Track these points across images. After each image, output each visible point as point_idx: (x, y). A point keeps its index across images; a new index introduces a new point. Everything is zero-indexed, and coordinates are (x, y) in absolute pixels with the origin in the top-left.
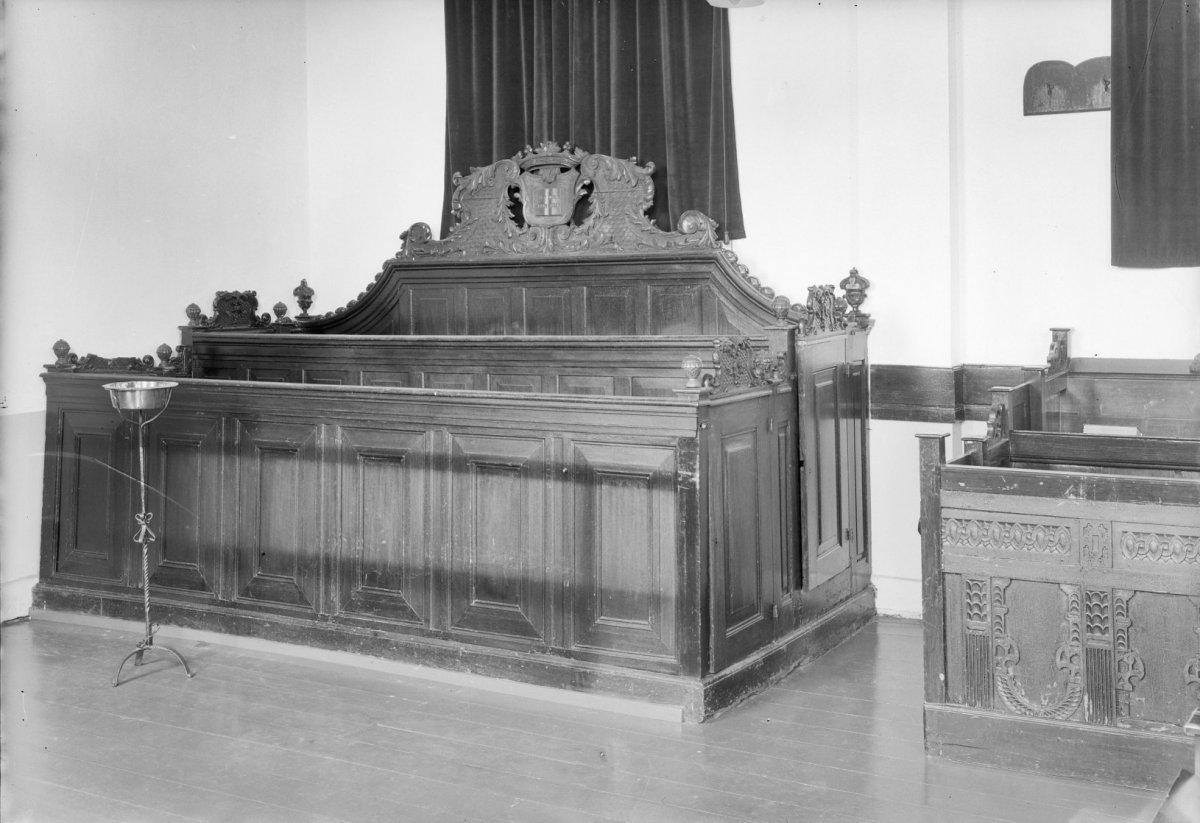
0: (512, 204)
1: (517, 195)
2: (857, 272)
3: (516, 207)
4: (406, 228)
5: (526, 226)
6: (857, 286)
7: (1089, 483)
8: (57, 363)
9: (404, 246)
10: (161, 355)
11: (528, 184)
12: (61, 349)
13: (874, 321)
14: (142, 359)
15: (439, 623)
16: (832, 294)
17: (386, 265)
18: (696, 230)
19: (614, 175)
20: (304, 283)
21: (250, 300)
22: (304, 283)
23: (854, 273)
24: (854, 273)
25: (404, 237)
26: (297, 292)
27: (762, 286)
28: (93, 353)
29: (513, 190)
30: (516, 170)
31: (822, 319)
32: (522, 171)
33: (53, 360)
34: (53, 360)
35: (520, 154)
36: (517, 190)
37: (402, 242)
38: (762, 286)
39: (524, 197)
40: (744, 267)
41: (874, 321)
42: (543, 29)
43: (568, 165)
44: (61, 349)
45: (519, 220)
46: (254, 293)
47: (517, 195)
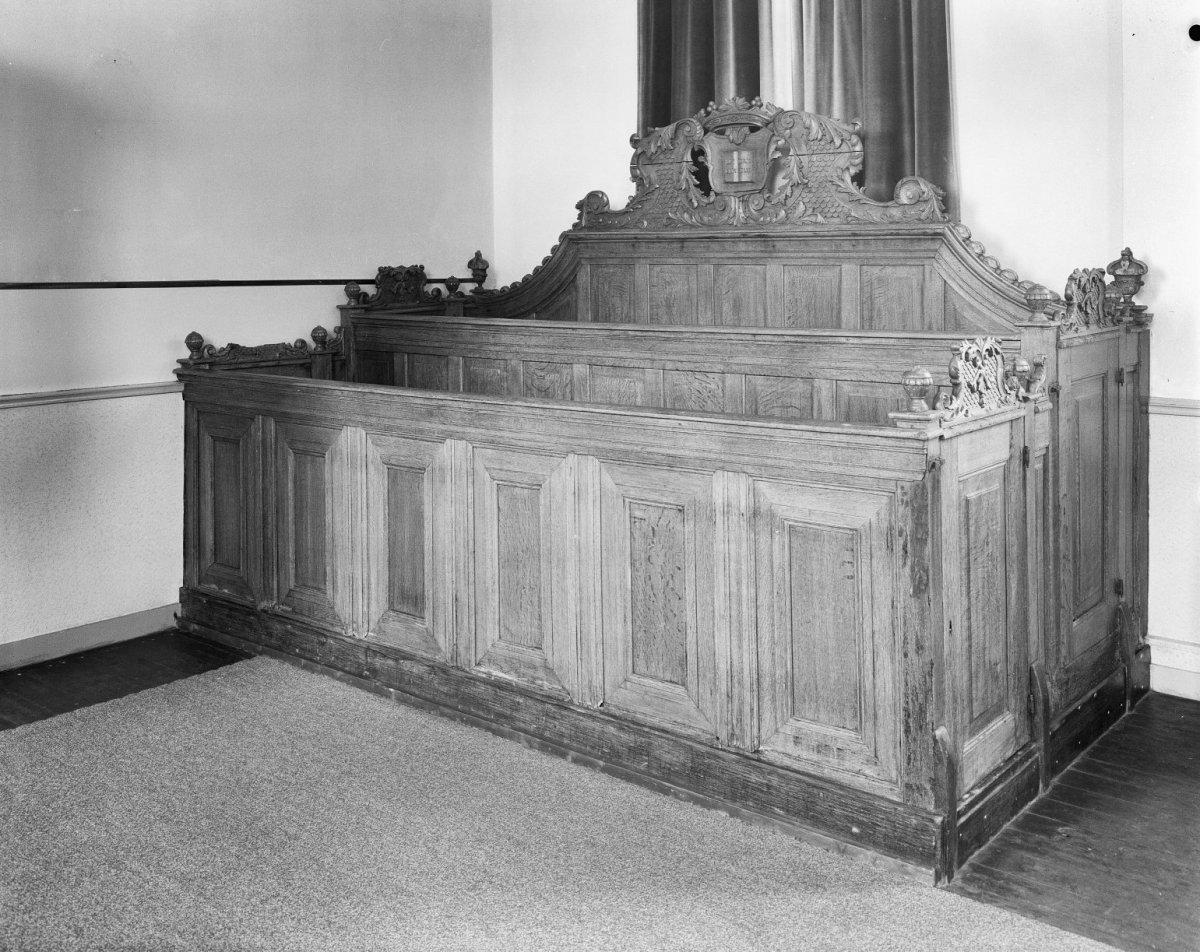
0: (695, 168)
1: (701, 159)
2: (1131, 254)
3: (701, 173)
4: (582, 196)
5: (712, 193)
6: (1132, 271)
7: (675, 228)
8: (191, 358)
9: (580, 217)
10: (314, 338)
11: (712, 147)
12: (195, 342)
13: (1152, 316)
14: (292, 344)
15: (581, 398)
16: (1100, 280)
17: (564, 236)
18: (919, 200)
19: (813, 135)
20: (478, 254)
21: (416, 275)
22: (478, 254)
23: (1127, 254)
24: (1127, 254)
25: (579, 206)
26: (471, 264)
27: (1002, 268)
28: (385, 265)
29: (698, 153)
30: (699, 130)
31: (1086, 313)
32: (706, 131)
33: (186, 354)
34: (186, 354)
35: (702, 111)
36: (702, 152)
37: (578, 212)
38: (1002, 268)
39: (712, 162)
40: (979, 244)
41: (1152, 316)
42: (652, 52)
43: (759, 124)
44: (195, 342)
45: (705, 187)
46: (422, 267)
47: (701, 159)
